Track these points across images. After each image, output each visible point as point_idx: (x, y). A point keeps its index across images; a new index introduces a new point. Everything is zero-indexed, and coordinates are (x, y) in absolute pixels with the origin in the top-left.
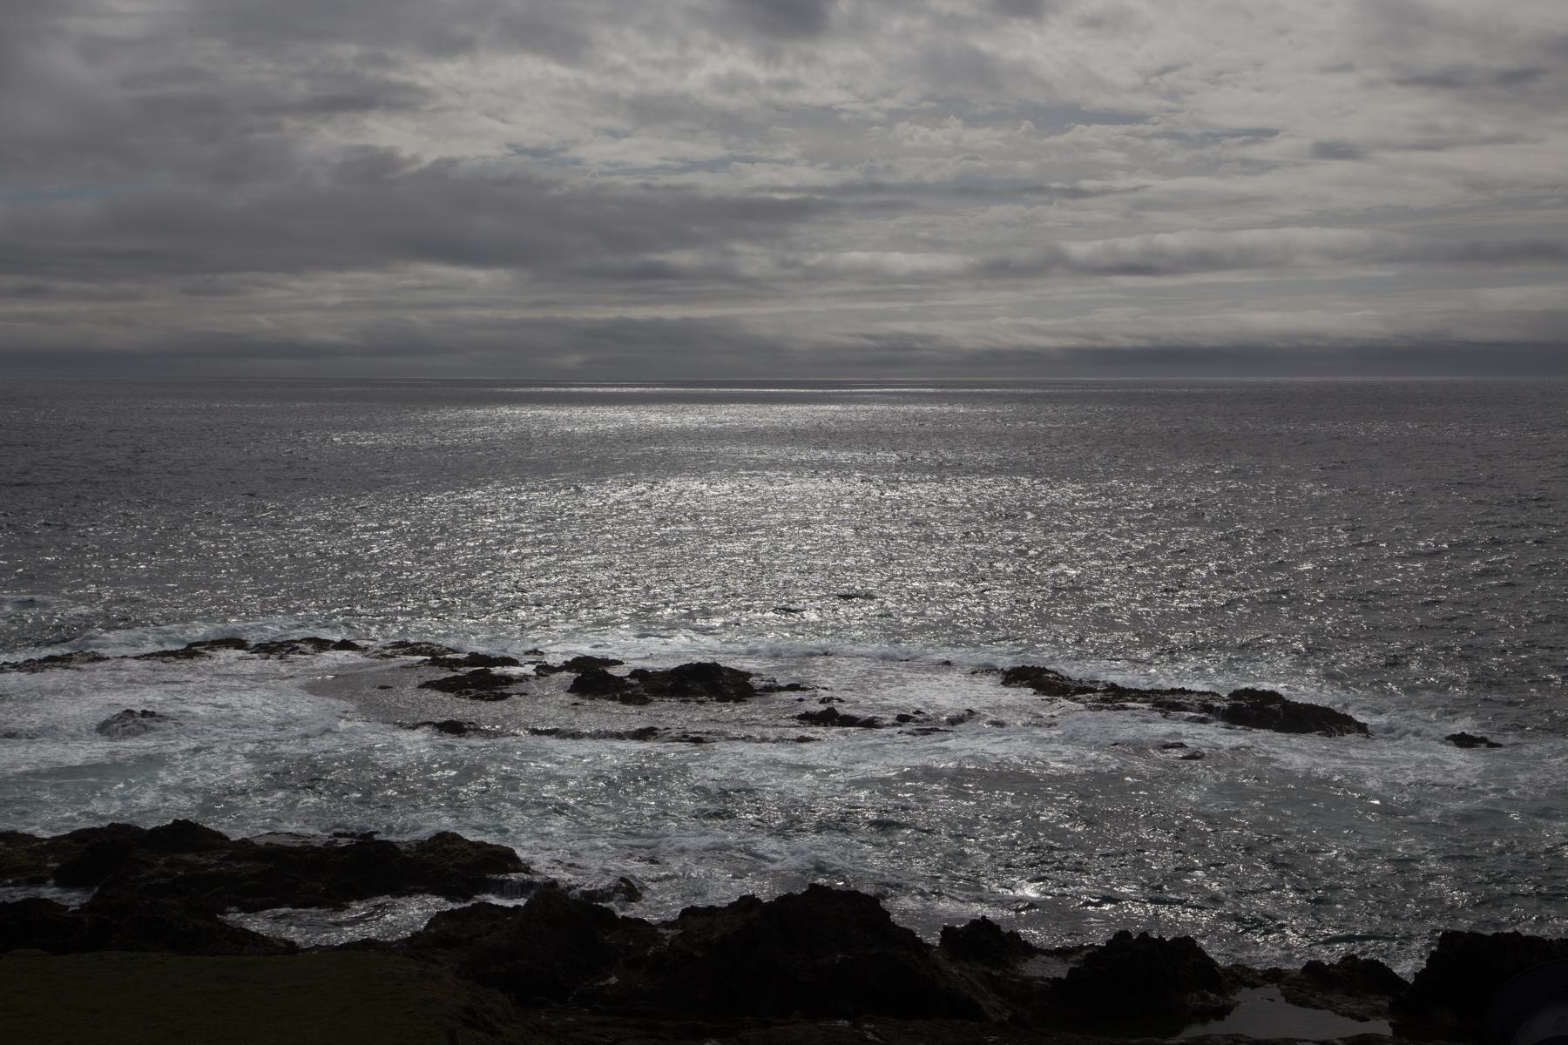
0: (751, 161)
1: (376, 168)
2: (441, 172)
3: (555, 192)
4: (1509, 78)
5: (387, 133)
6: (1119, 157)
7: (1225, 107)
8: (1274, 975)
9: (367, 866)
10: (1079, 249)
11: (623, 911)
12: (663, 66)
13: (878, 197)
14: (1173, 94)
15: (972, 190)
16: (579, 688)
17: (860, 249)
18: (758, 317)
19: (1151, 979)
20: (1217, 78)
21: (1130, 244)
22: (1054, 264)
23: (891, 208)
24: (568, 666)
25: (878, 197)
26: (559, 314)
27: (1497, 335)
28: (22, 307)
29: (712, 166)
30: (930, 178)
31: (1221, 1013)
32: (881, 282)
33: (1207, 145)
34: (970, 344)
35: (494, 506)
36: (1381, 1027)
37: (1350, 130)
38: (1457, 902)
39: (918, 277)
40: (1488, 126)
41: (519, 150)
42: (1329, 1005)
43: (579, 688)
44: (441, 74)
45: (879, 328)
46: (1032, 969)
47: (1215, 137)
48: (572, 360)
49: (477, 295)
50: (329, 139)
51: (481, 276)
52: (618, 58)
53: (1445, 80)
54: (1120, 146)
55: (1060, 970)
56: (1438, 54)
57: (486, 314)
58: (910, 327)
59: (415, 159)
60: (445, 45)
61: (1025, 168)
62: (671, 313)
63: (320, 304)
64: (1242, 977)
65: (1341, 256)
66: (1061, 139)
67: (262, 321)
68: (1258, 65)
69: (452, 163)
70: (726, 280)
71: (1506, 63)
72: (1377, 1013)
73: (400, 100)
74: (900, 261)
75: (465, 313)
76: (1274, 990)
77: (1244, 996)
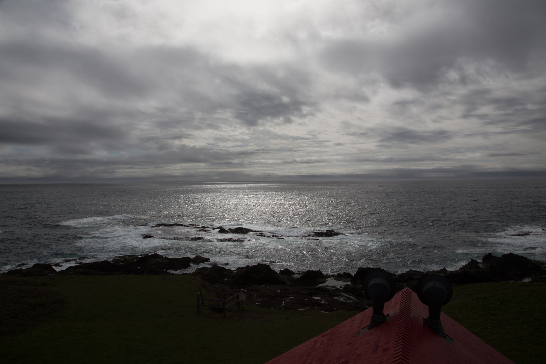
0: (247, 145)
1: (184, 147)
2: (193, 148)
3: (212, 151)
4: (363, 134)
5: (187, 142)
6: (305, 145)
7: (322, 137)
8: (333, 276)
9: (185, 262)
10: (298, 159)
11: (227, 267)
12: (232, 131)
13: (265, 151)
14: (313, 135)
15: (279, 150)
16: (220, 232)
17: (261, 159)
18: (247, 170)
19: (313, 277)
20: (320, 133)
21: (305, 159)
22: (294, 162)
23: (266, 153)
24: (218, 228)
25: (265, 151)
26: (215, 170)
27: (362, 173)
28: (130, 170)
29: (241, 146)
30: (276, 148)
31: (324, 282)
32: (266, 164)
33: (320, 143)
34: (281, 175)
35: (191, 196)
36: (349, 283)
37: (341, 141)
38: (362, 263)
39: (273, 164)
40: (361, 141)
41: (209, 144)
42: (341, 280)
43: (220, 232)
44: (196, 133)
45: (266, 172)
46: (295, 276)
47: (321, 142)
48: (216, 178)
49: (201, 168)
50: (177, 142)
51: (202, 164)
52: (225, 130)
53: (353, 134)
54: (306, 143)
55: (299, 276)
56: (353, 130)
57: (203, 170)
58: (271, 172)
59: (189, 146)
60: (197, 128)
61: (290, 146)
62: (233, 170)
63: (177, 169)
64: (328, 276)
65: (338, 160)
66: (296, 142)
67: (166, 172)
68: (326, 131)
69: (195, 146)
70: (241, 165)
71: (362, 132)
72: (348, 281)
73: (187, 136)
74: (270, 161)
75: (199, 170)
76: (333, 278)
77: (328, 279)
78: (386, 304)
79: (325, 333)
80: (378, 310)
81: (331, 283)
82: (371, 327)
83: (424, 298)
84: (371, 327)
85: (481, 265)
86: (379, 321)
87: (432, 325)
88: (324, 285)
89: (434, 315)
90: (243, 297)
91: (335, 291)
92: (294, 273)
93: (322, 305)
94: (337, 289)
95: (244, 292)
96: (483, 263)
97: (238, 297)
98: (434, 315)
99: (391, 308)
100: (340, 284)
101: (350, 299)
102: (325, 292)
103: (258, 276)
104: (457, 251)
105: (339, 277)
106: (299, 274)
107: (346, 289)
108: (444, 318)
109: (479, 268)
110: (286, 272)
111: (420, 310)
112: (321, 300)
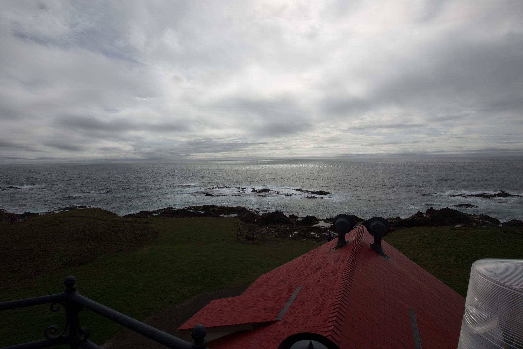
8: (323, 220)
19: (311, 220)
46: (299, 219)
55: (301, 219)
64: (320, 220)
78: (346, 234)
79: (311, 251)
80: (342, 238)
81: (321, 224)
82: (337, 248)
83: (370, 231)
84: (337, 248)
85: (425, 216)
86: (342, 244)
87: (376, 249)
88: (317, 225)
89: (377, 242)
90: (265, 231)
91: (325, 229)
92: (298, 218)
93: (315, 238)
94: (326, 228)
95: (266, 228)
96: (426, 214)
97: (262, 231)
98: (377, 242)
99: (350, 237)
100: (328, 225)
101: (334, 234)
102: (317, 229)
103: (276, 218)
104: (343, 198)
105: (327, 221)
106: (302, 218)
107: (331, 228)
108: (384, 244)
109: (423, 217)
110: (294, 217)
111: (369, 239)
112: (315, 235)
